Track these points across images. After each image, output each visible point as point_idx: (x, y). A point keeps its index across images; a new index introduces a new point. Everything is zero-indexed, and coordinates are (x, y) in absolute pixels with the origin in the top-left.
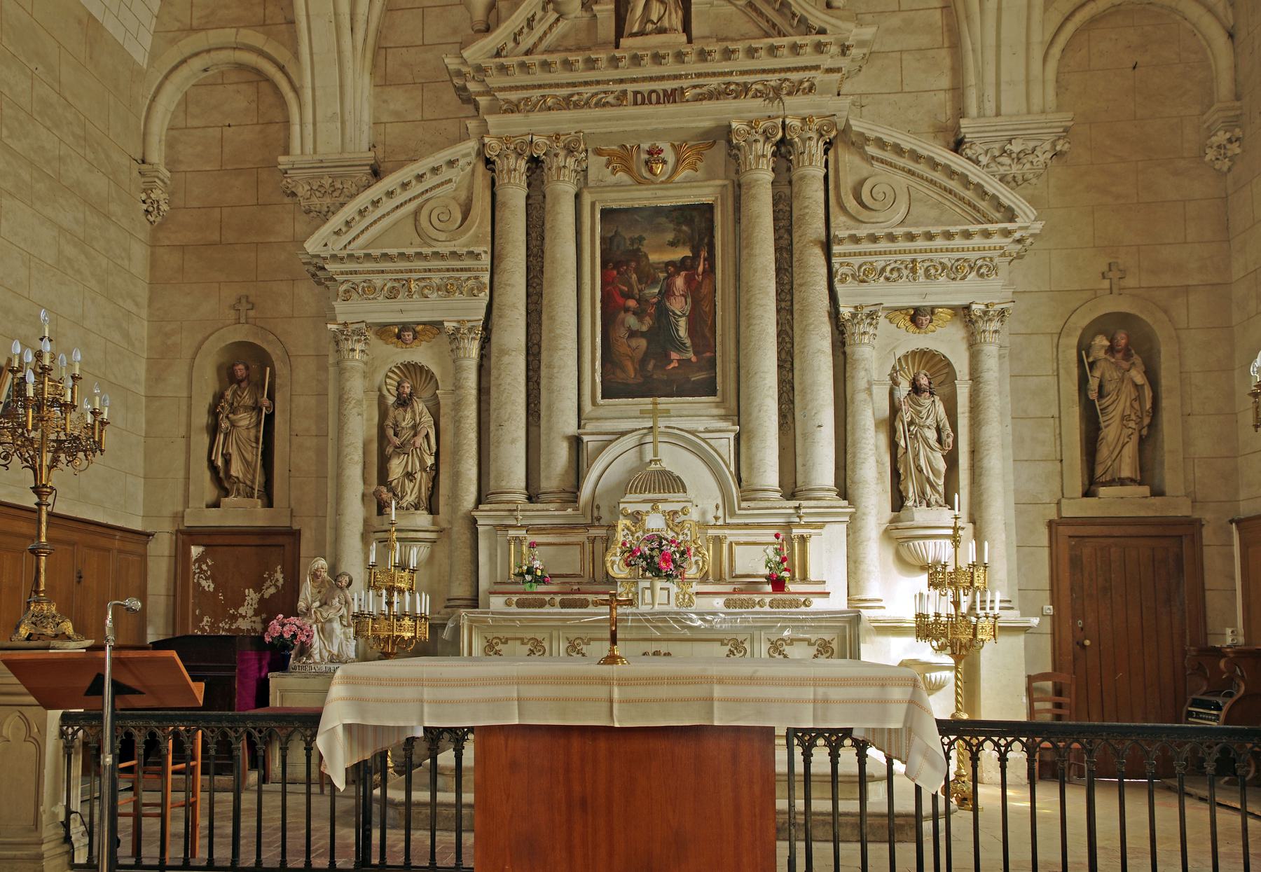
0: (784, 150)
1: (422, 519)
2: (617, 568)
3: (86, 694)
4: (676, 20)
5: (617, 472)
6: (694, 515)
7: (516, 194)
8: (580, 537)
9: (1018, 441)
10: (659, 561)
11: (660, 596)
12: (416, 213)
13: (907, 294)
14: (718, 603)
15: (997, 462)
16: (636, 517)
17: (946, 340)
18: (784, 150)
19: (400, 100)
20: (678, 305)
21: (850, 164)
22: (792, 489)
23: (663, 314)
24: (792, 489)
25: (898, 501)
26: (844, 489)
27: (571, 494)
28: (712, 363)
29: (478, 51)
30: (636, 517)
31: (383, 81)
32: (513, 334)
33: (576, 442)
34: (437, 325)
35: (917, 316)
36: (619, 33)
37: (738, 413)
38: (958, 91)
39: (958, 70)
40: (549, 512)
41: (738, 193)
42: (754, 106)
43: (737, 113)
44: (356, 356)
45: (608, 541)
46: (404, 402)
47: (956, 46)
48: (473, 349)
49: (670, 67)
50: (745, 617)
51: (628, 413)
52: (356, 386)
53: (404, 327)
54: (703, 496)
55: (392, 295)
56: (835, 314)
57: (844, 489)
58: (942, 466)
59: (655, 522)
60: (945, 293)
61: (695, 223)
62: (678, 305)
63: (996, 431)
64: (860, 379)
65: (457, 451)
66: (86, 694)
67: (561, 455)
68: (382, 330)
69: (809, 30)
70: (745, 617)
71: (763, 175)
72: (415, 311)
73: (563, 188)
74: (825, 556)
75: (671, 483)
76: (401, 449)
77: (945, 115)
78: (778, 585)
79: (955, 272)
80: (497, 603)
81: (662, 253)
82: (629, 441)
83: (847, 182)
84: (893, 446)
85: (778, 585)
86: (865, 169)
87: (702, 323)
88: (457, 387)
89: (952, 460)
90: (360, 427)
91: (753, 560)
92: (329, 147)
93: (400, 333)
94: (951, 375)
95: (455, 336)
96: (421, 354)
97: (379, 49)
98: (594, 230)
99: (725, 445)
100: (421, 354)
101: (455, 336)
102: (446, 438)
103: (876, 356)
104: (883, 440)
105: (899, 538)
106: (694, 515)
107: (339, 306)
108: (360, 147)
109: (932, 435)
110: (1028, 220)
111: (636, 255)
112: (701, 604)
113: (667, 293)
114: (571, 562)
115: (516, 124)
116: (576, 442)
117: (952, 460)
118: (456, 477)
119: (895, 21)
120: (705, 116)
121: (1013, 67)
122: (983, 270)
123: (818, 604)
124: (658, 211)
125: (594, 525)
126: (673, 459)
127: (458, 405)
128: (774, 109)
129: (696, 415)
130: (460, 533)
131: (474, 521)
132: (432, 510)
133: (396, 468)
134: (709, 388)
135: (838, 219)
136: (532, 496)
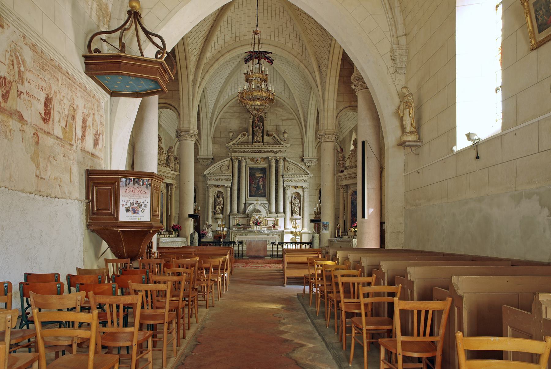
0: (277, 161)
1: (221, 215)
2: (251, 223)
3: (77, 268)
4: (261, 140)
5: (251, 209)
6: (262, 216)
7: (236, 166)
8: (246, 219)
9: (310, 205)
10: (257, 223)
11: (257, 228)
12: (221, 168)
13: (294, 184)
14: (266, 229)
15: (306, 209)
16: (254, 217)
17: (300, 191)
18: (277, 161)
19: (217, 146)
20: (261, 183)
21: (287, 164)
22: (277, 212)
23: (258, 185)
24: (277, 212)
25: (292, 214)
26: (284, 212)
27: (244, 212)
28: (266, 193)
29: (231, 144)
30: (254, 217)
31: (214, 143)
32: (236, 187)
33: (245, 204)
34: (223, 186)
35: (295, 187)
36: (252, 142)
37: (269, 200)
38: (303, 151)
39: (303, 148)
40: (241, 215)
41: (270, 167)
42: (273, 154)
43: (270, 155)
44: (211, 190)
45: (250, 220)
46: (218, 197)
47: (303, 145)
48: (229, 189)
49: (260, 147)
50: (269, 231)
51: (252, 200)
52: (211, 194)
53: (218, 185)
54: (264, 213)
55: (217, 180)
56: (283, 186)
57: (284, 212)
58: (298, 209)
59: (257, 217)
60: (299, 184)
61: (263, 170)
62: (261, 183)
63: (306, 204)
64: (287, 196)
65: (227, 205)
66: (77, 268)
67: (243, 206)
68: (215, 186)
69: (281, 144)
70: (269, 231)
71: (274, 165)
72: (220, 183)
73: (244, 165)
74: (281, 222)
75: (259, 211)
76: (218, 205)
77: (301, 155)
78: (274, 226)
79: (301, 181)
80: (234, 229)
81: (258, 175)
82: (253, 205)
83: (286, 166)
84: (292, 206)
85: (274, 226)
86: (289, 165)
87: (264, 186)
88: (227, 195)
89: (300, 208)
90: (211, 201)
91: (271, 223)
92: (205, 154)
93: (218, 186)
94: (300, 196)
95: (227, 187)
96: (221, 189)
97: (214, 138)
98: (248, 171)
99: (267, 206)
100: (221, 189)
101: (227, 187)
102: (225, 203)
103: (290, 193)
104: (290, 205)
105: (292, 219)
106: (262, 216)
107: (208, 182)
108: (210, 155)
109: (297, 205)
110: (310, 175)
111: (255, 175)
112: (263, 229)
113: (259, 181)
114: (244, 222)
115: (237, 155)
116: (245, 204)
117: (300, 208)
118: (226, 209)
119: (294, 140)
120: (265, 155)
121: (311, 150)
122: (305, 181)
123: (279, 229)
124: (258, 168)
125: (248, 217)
126: (260, 208)
127: (227, 198)
128: (276, 155)
129: (263, 201)
130: (227, 217)
131: (229, 216)
132: (222, 214)
133: (217, 207)
134: (265, 196)
135: (285, 172)
136: (238, 212)
